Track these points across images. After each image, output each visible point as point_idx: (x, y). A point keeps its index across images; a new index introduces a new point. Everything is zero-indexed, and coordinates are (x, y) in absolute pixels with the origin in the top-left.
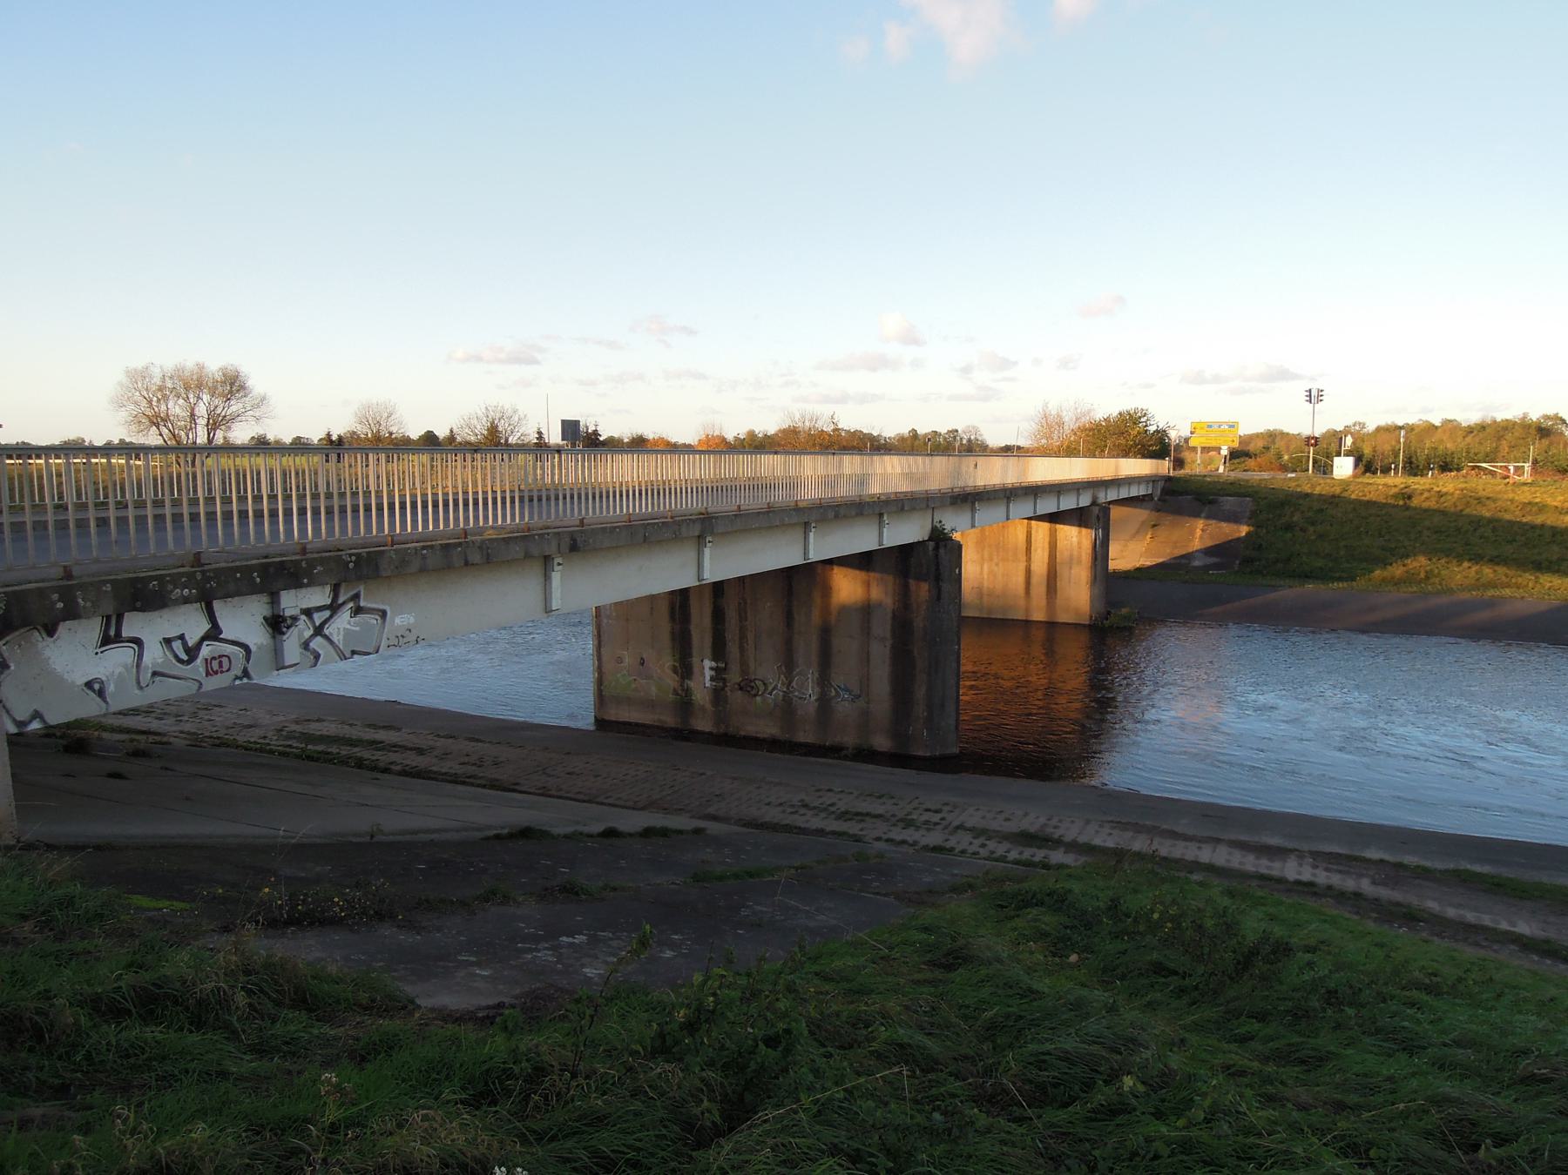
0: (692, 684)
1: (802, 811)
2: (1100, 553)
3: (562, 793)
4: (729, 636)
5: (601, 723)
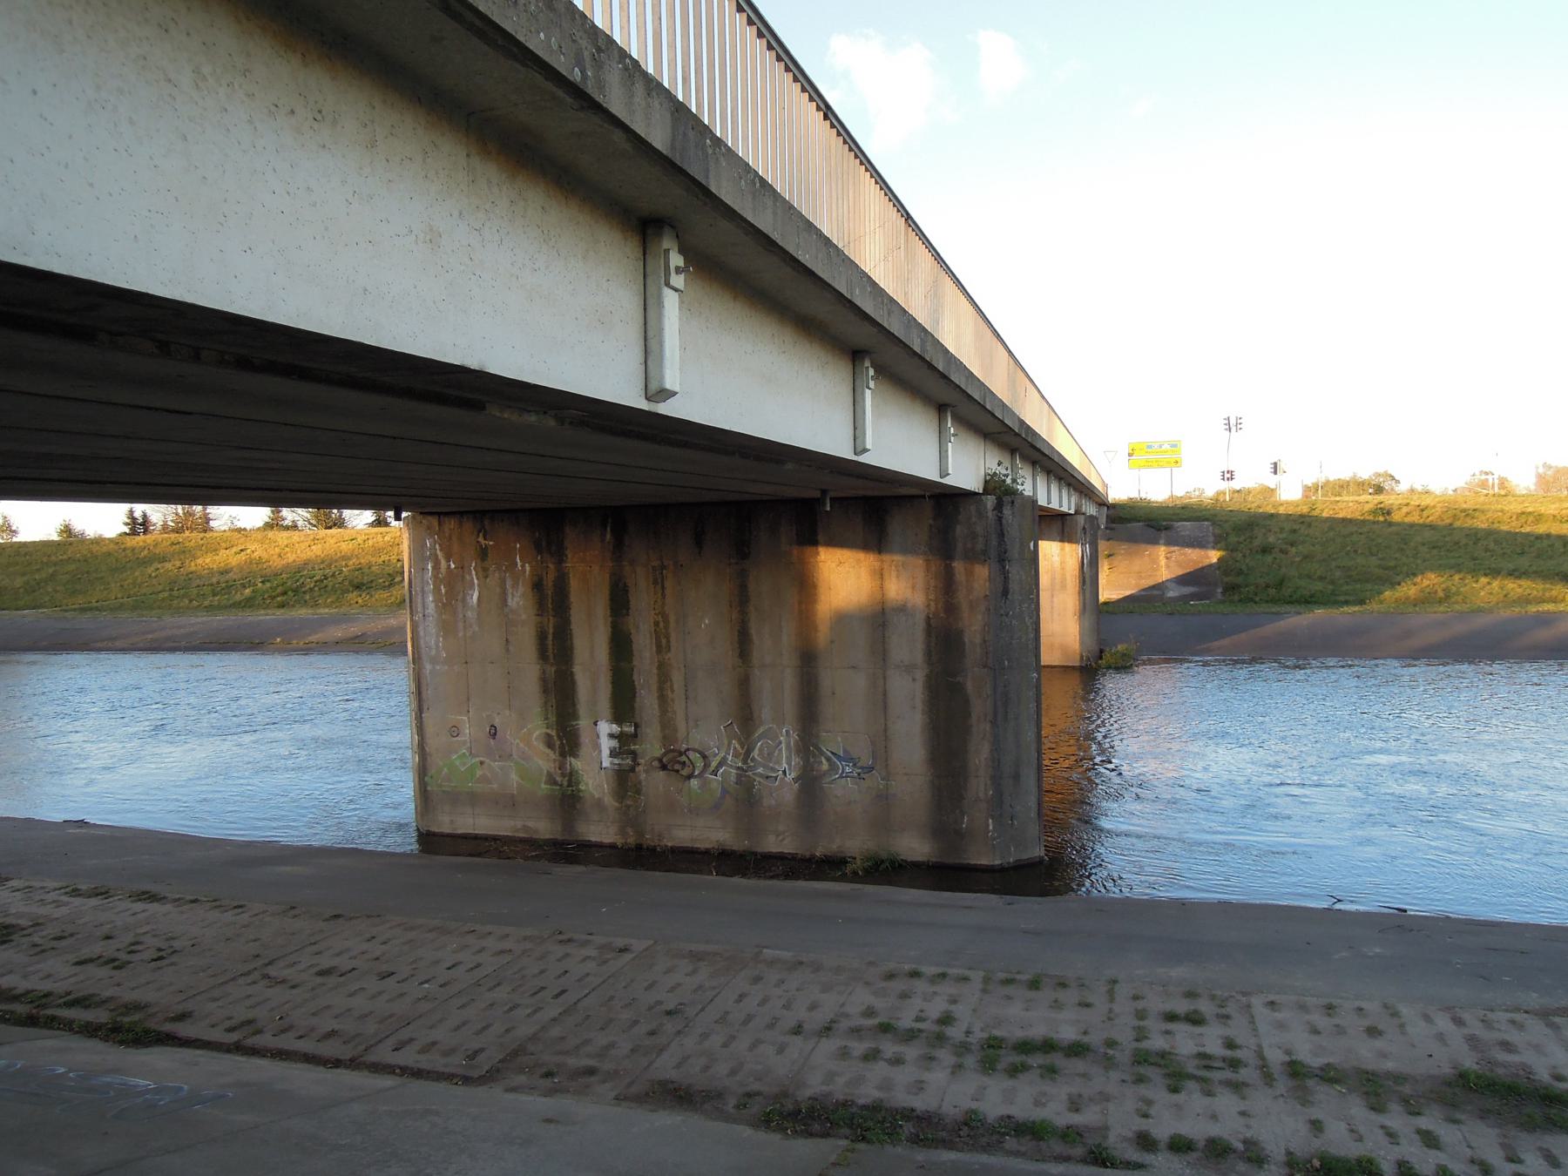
0: (577, 764)
1: (889, 1048)
2: (1088, 578)
3: (288, 1042)
4: (639, 680)
5: (430, 841)
